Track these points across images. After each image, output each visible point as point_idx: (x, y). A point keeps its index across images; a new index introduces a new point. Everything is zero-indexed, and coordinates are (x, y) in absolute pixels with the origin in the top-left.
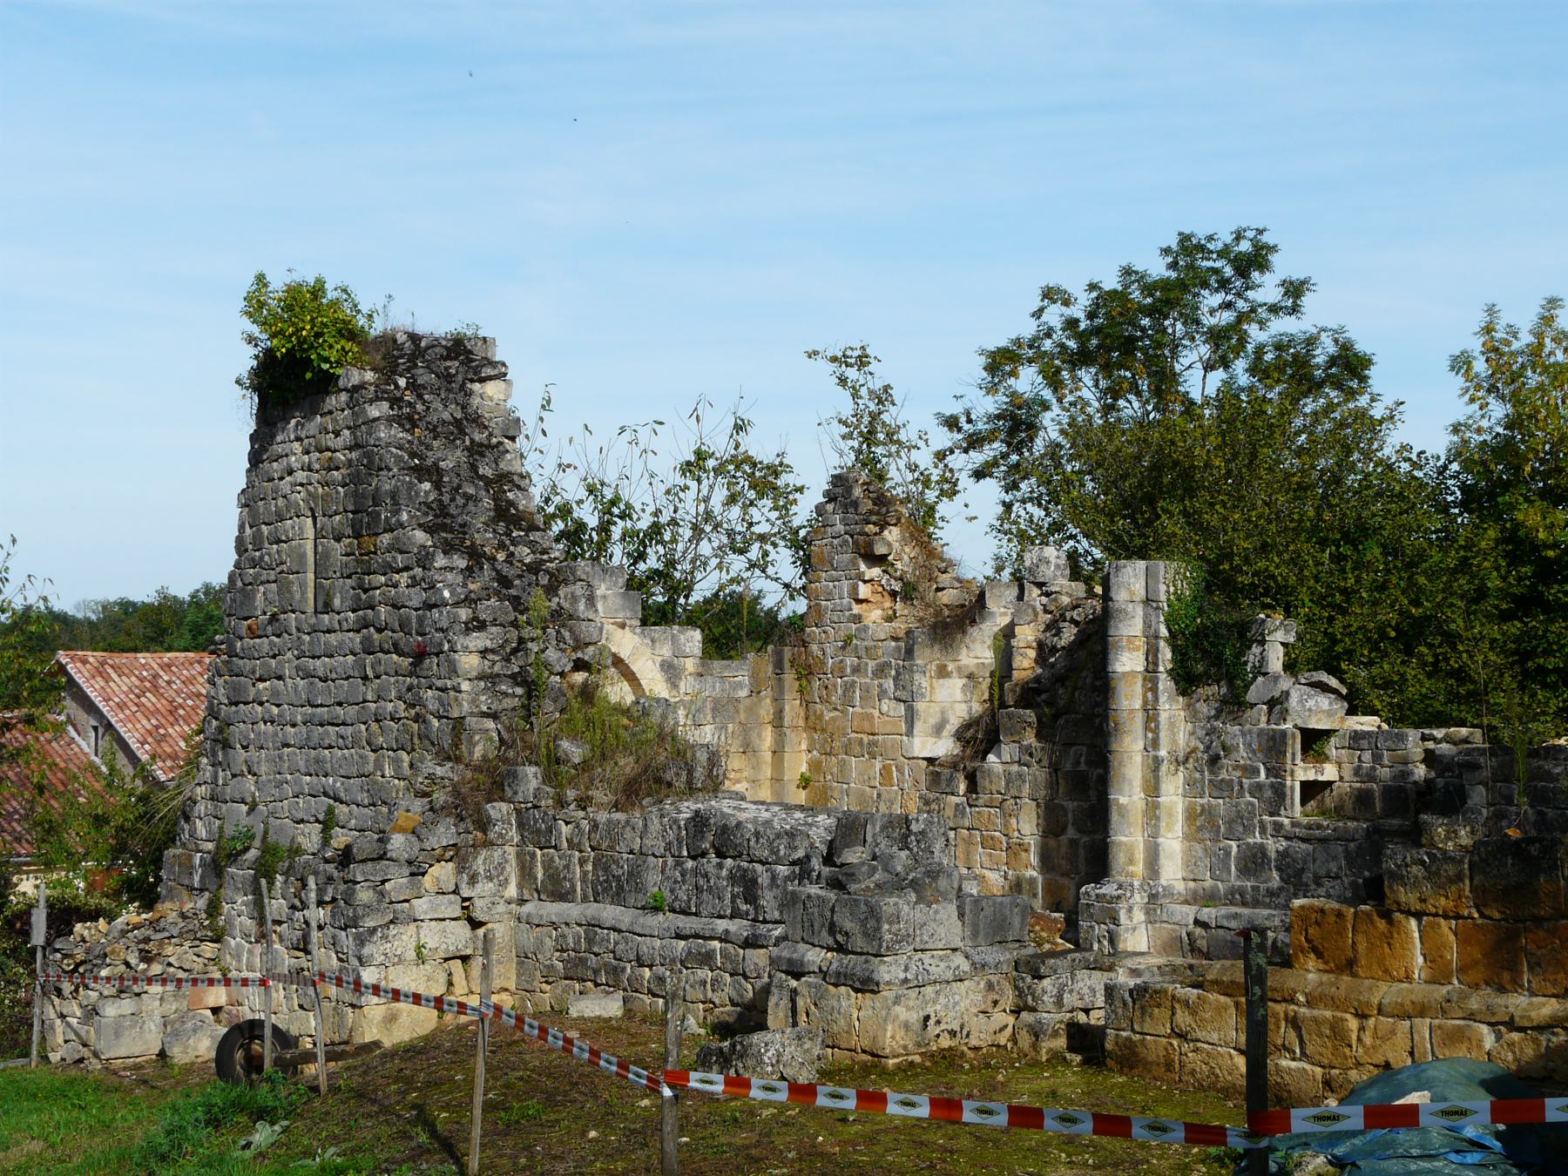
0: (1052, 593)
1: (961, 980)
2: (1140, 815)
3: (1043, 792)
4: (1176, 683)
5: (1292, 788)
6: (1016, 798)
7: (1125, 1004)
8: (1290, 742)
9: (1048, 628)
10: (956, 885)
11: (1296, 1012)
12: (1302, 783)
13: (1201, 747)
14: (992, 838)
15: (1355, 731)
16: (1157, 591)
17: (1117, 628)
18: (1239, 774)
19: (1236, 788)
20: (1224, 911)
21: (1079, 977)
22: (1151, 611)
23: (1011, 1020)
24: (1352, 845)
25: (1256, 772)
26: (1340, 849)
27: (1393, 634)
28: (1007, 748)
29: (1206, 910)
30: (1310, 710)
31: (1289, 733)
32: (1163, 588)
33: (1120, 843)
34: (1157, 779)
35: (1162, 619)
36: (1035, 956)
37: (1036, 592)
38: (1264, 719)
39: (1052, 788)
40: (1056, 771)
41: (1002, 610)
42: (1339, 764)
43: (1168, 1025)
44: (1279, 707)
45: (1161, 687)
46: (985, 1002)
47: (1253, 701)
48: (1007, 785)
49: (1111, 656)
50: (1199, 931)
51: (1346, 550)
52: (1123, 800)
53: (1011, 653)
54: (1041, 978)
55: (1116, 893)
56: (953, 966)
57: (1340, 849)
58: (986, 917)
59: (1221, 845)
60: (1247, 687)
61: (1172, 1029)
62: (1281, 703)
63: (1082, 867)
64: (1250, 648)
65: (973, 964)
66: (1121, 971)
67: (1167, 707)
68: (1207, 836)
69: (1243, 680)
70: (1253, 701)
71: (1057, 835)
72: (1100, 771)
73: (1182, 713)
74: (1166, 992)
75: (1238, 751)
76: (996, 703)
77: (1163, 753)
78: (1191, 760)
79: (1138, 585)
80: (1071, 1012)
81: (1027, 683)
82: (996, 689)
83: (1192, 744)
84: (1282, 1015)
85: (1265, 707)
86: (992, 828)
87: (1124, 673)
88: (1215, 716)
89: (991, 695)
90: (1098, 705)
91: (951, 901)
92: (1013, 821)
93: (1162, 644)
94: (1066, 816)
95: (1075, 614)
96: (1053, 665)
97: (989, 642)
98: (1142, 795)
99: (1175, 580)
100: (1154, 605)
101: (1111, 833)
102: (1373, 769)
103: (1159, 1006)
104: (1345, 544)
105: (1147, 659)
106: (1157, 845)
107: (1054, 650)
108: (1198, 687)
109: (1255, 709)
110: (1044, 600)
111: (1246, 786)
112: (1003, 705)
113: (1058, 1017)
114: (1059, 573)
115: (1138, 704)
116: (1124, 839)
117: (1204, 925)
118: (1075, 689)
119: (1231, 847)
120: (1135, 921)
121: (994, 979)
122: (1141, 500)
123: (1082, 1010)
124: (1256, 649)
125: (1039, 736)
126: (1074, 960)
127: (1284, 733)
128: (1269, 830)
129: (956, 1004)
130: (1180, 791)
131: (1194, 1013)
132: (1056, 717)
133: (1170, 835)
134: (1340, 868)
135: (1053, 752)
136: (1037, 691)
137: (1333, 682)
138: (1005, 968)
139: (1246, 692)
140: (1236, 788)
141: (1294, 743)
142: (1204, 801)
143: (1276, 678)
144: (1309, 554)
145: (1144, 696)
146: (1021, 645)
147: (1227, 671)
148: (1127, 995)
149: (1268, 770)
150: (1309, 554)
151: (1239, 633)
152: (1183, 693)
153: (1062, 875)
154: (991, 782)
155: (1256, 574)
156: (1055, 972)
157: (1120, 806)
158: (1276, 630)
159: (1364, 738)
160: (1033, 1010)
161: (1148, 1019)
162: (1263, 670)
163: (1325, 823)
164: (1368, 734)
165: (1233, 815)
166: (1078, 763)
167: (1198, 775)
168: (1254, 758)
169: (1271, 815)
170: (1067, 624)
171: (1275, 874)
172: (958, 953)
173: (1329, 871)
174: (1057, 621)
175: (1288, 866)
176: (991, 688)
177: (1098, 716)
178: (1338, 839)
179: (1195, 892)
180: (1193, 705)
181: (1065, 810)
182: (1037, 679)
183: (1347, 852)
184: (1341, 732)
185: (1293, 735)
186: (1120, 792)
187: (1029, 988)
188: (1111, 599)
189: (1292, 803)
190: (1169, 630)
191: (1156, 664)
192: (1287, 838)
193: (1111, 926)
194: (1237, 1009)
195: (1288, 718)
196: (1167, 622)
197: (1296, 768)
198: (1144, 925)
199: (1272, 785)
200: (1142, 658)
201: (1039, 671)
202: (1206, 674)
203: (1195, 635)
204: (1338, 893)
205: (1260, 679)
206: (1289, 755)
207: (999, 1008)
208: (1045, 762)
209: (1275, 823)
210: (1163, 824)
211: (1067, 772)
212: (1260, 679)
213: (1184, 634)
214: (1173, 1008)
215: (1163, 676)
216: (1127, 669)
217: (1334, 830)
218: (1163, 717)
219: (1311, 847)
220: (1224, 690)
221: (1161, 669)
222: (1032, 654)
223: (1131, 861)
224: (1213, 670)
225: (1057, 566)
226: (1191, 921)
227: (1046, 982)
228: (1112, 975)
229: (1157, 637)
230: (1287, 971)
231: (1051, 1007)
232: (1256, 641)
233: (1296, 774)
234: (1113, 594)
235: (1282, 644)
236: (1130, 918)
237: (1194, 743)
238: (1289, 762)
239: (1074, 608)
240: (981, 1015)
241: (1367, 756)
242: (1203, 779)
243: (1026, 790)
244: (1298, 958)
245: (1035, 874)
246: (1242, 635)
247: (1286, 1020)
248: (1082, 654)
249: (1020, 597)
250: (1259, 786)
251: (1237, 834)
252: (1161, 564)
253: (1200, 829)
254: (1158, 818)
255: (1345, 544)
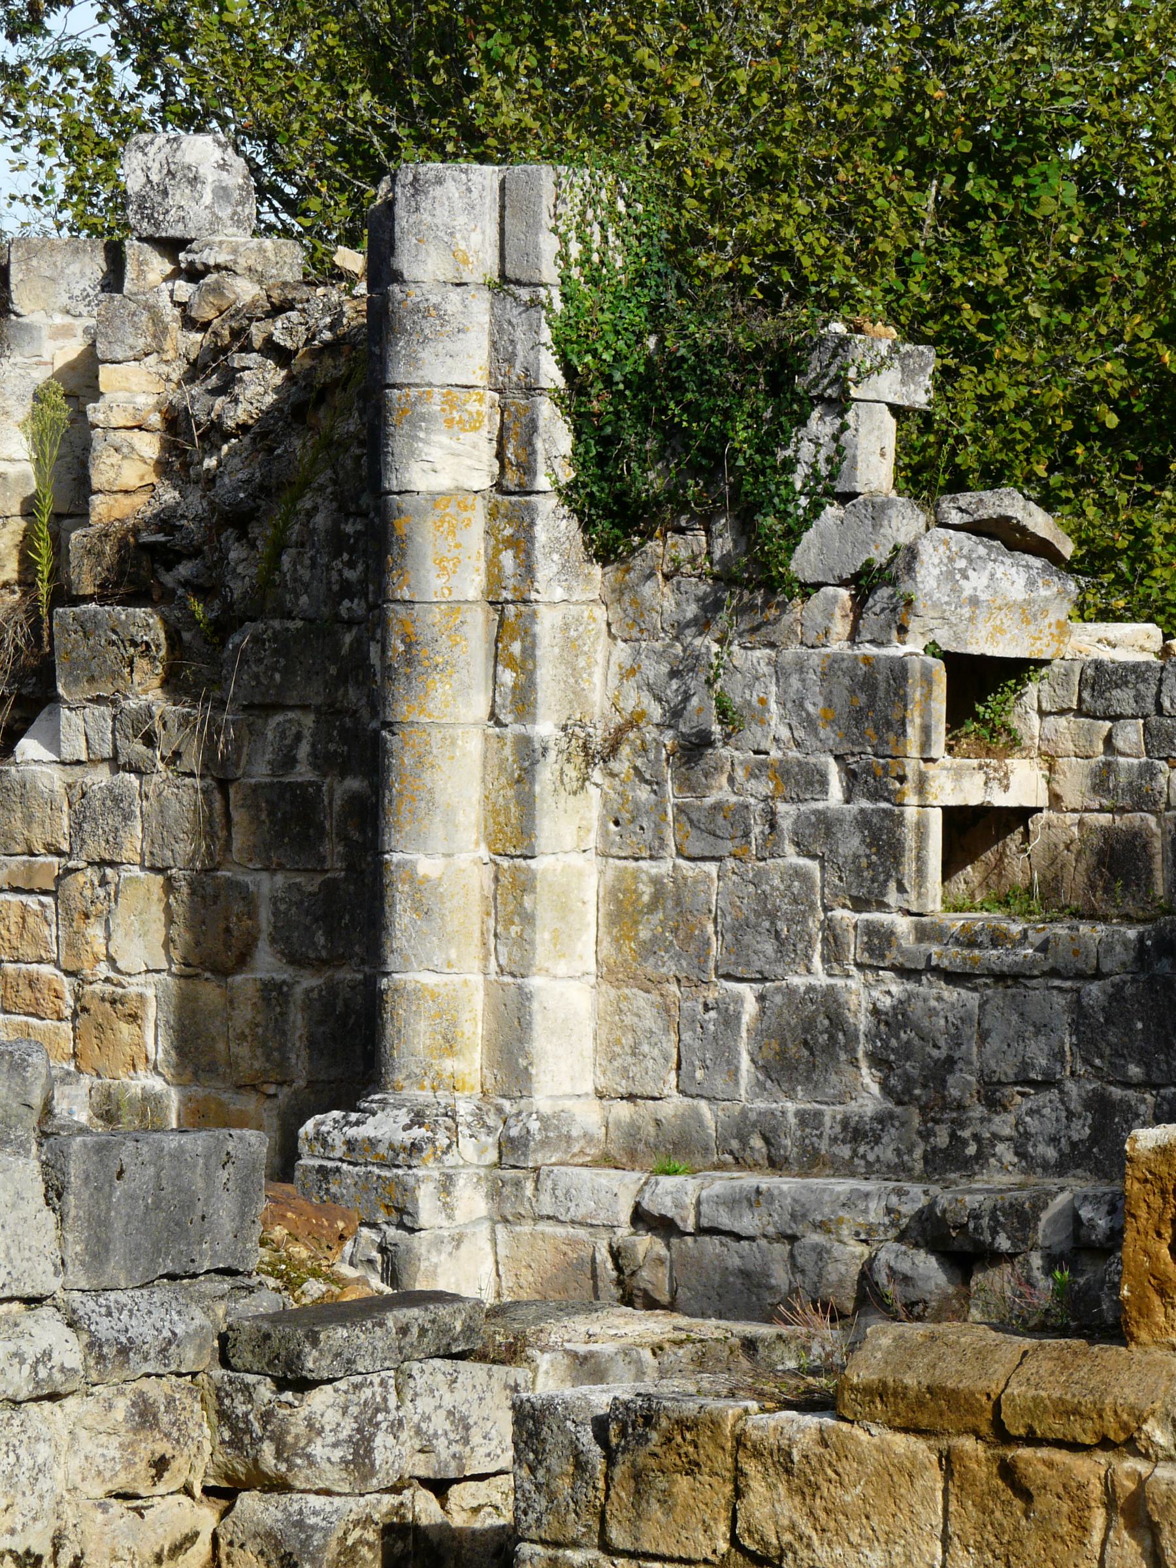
0: (207, 269)
1: (54, 1397)
2: (476, 910)
3: (184, 848)
4: (586, 526)
5: (921, 829)
6: (103, 863)
7: (581, 1465)
8: (916, 694)
9: (195, 370)
10: (37, 1100)
11: (1142, 1482)
12: (948, 811)
13: (656, 712)
14: (32, 982)
15: (1098, 665)
16: (532, 255)
17: (413, 360)
18: (764, 787)
19: (758, 829)
20: (720, 1184)
21: (420, 1382)
22: (513, 313)
23: (206, 1517)
24: (1095, 991)
25: (816, 781)
26: (1059, 1001)
27: (1112, 421)
28: (76, 719)
29: (667, 1182)
30: (974, 601)
31: (915, 666)
32: (549, 245)
33: (419, 992)
34: (527, 804)
35: (546, 335)
36: (280, 1317)
37: (159, 265)
38: (841, 627)
39: (211, 835)
40: (223, 785)
41: (59, 319)
42: (1051, 762)
43: (722, 1528)
44: (884, 592)
45: (541, 534)
46: (129, 1464)
47: (809, 575)
48: (77, 827)
49: (397, 444)
50: (646, 1244)
51: (979, 188)
52: (427, 866)
53: (86, 447)
54: (304, 1385)
55: (407, 1137)
56: (31, 1352)
57: (1059, 1001)
58: (131, 1197)
59: (712, 995)
60: (793, 535)
61: (734, 1541)
62: (893, 582)
63: (300, 1064)
64: (802, 421)
65: (94, 1345)
66: (544, 1361)
67: (559, 593)
68: (670, 968)
69: (783, 515)
70: (809, 576)
71: (222, 972)
72: (354, 784)
73: (600, 613)
74: (715, 1424)
75: (763, 722)
76: (44, 589)
77: (545, 728)
78: (625, 750)
79: (476, 238)
80: (395, 1490)
81: (136, 531)
82: (44, 547)
83: (629, 705)
84: (1096, 1490)
85: (844, 594)
86: (29, 951)
87: (434, 496)
88: (695, 621)
89: (27, 565)
90: (347, 590)
91: (21, 1148)
92: (95, 931)
93: (547, 410)
94: (252, 914)
95: (277, 330)
96: (211, 480)
97: (22, 410)
98: (484, 853)
99: (584, 222)
100: (525, 294)
101: (393, 962)
102: (1149, 772)
103: (692, 1468)
104: (980, 171)
105: (500, 455)
106: (524, 997)
107: (215, 433)
108: (647, 535)
109: (817, 599)
110: (184, 290)
111: (786, 824)
112: (64, 596)
113: (356, 1506)
114: (225, 213)
115: (473, 585)
116: (428, 979)
117: (664, 1227)
118: (279, 547)
119: (739, 1000)
120: (460, 1216)
121: (155, 1390)
122: (423, 40)
123: (426, 1483)
124: (820, 425)
125: (172, 684)
126: (404, 1330)
127: (899, 671)
128: (853, 949)
129: (40, 1470)
130: (592, 840)
131: (806, 1490)
132: (222, 628)
133: (562, 968)
134: (1058, 1056)
135: (215, 729)
136: (165, 556)
137: (1040, 522)
138: (189, 1358)
139: (791, 550)
140: (758, 829)
141: (928, 696)
142: (663, 868)
143: (878, 510)
144: (888, 193)
145: (493, 563)
146: (118, 419)
147: (736, 488)
148: (586, 1436)
149: (851, 776)
150: (888, 193)
151: (771, 378)
152: (604, 554)
153: (239, 1087)
154: (28, 820)
155: (745, 247)
156: (349, 1367)
157: (417, 884)
158: (877, 369)
159: (1123, 683)
160: (280, 1486)
161: (656, 1510)
162: (840, 487)
163: (1016, 928)
164: (1131, 673)
165: (747, 907)
166: (288, 761)
167: (643, 794)
168: (811, 742)
169: (859, 905)
170: (253, 359)
171: (868, 1078)
172: (45, 1311)
173: (1025, 1066)
174: (225, 350)
175: (907, 1052)
176: (26, 546)
177: (350, 623)
178: (1054, 973)
179: (632, 1132)
180: (632, 588)
181: (248, 898)
182: (165, 521)
183: (1079, 1012)
184: (1057, 667)
185: (927, 679)
186: (420, 841)
187: (267, 1417)
188: (397, 277)
189: (921, 872)
190: (569, 371)
191: (527, 469)
192: (904, 973)
193: (392, 1233)
194: (948, 1474)
195: (914, 625)
196: (561, 343)
197: (931, 770)
198: (484, 1229)
199: (864, 821)
200: (488, 451)
201: (170, 496)
202: (674, 498)
203: (642, 383)
204: (1050, 1128)
205: (832, 512)
206: (913, 733)
207: (172, 1480)
208: (192, 760)
209: (871, 930)
210: (542, 937)
211: (255, 788)
212: (832, 512)
213: (608, 381)
214: (738, 1473)
215: (548, 505)
216: (442, 482)
217: (1043, 947)
218: (547, 623)
219: (972, 999)
220: (724, 545)
221: (543, 482)
222: (149, 446)
223: (450, 1045)
224: (693, 488)
225: (222, 192)
226: (625, 1215)
227: (319, 1400)
228: (518, 1374)
229: (531, 389)
230: (1112, 1354)
231: (333, 1477)
232: (821, 399)
233: (933, 787)
234: (404, 262)
235: (897, 411)
236: (448, 1209)
237: (635, 699)
238: (913, 750)
239: (277, 310)
240: (118, 1506)
241: (1131, 735)
242: (660, 805)
243: (134, 841)
244: (1145, 1312)
245: (157, 1084)
246: (778, 385)
247: (1110, 1503)
248: (298, 446)
249: (113, 280)
250: (826, 824)
251: (758, 963)
252: (546, 174)
253: (648, 949)
254: (528, 919)
255: (980, 171)
